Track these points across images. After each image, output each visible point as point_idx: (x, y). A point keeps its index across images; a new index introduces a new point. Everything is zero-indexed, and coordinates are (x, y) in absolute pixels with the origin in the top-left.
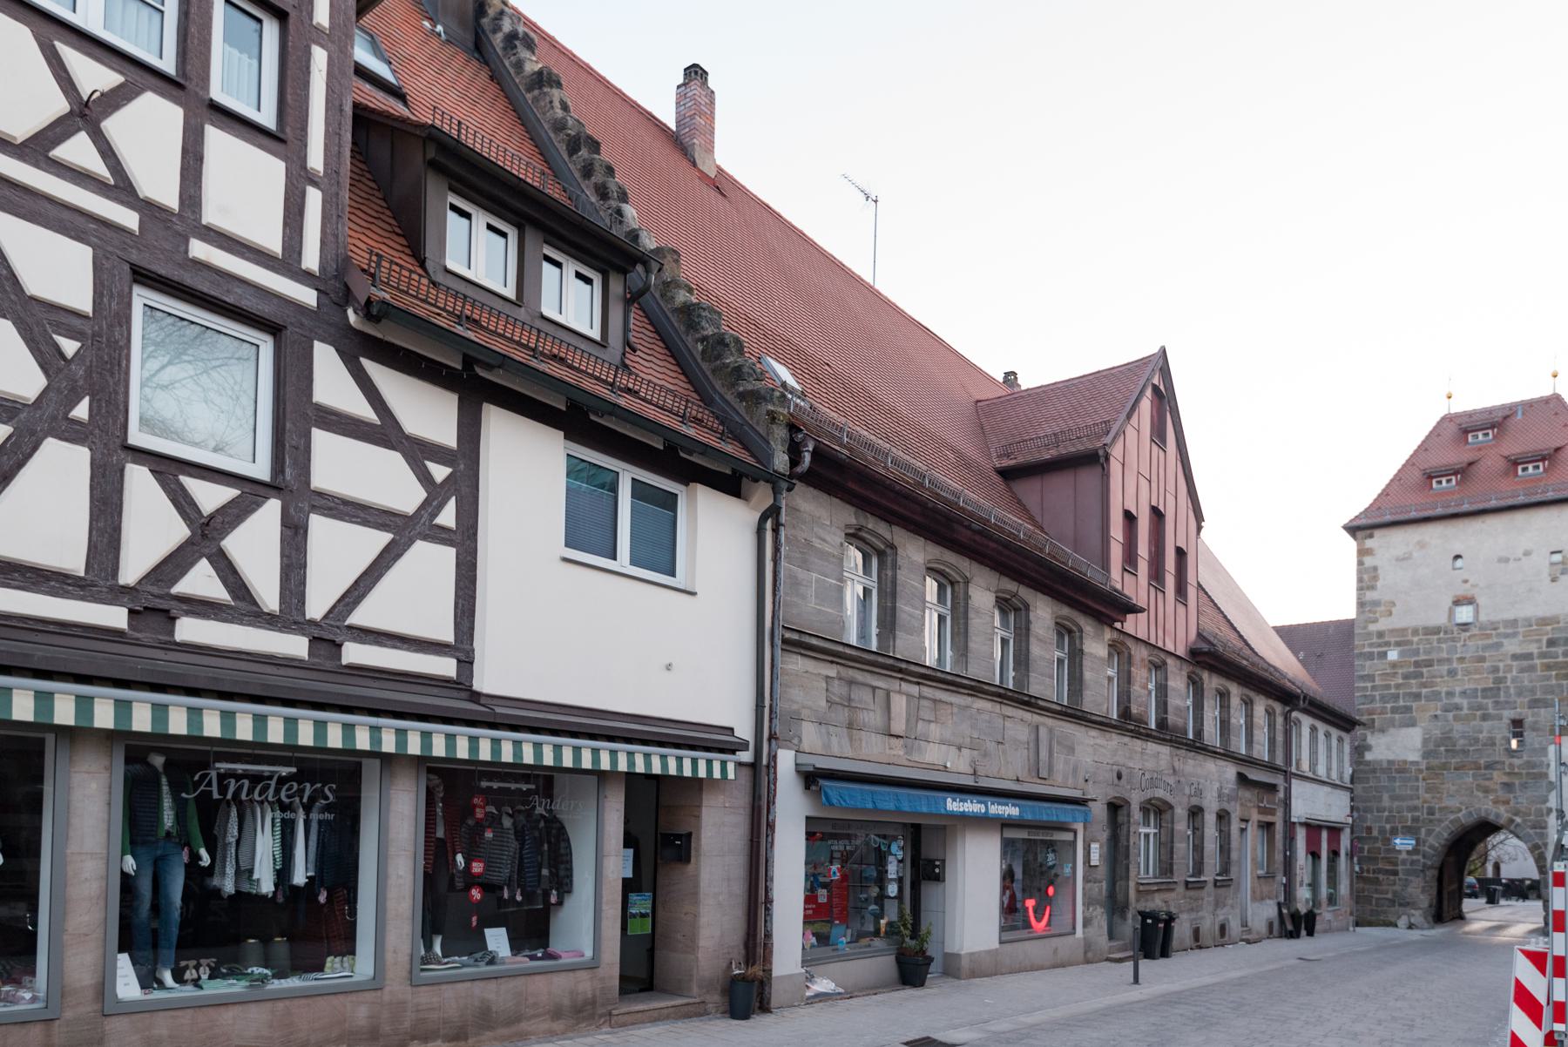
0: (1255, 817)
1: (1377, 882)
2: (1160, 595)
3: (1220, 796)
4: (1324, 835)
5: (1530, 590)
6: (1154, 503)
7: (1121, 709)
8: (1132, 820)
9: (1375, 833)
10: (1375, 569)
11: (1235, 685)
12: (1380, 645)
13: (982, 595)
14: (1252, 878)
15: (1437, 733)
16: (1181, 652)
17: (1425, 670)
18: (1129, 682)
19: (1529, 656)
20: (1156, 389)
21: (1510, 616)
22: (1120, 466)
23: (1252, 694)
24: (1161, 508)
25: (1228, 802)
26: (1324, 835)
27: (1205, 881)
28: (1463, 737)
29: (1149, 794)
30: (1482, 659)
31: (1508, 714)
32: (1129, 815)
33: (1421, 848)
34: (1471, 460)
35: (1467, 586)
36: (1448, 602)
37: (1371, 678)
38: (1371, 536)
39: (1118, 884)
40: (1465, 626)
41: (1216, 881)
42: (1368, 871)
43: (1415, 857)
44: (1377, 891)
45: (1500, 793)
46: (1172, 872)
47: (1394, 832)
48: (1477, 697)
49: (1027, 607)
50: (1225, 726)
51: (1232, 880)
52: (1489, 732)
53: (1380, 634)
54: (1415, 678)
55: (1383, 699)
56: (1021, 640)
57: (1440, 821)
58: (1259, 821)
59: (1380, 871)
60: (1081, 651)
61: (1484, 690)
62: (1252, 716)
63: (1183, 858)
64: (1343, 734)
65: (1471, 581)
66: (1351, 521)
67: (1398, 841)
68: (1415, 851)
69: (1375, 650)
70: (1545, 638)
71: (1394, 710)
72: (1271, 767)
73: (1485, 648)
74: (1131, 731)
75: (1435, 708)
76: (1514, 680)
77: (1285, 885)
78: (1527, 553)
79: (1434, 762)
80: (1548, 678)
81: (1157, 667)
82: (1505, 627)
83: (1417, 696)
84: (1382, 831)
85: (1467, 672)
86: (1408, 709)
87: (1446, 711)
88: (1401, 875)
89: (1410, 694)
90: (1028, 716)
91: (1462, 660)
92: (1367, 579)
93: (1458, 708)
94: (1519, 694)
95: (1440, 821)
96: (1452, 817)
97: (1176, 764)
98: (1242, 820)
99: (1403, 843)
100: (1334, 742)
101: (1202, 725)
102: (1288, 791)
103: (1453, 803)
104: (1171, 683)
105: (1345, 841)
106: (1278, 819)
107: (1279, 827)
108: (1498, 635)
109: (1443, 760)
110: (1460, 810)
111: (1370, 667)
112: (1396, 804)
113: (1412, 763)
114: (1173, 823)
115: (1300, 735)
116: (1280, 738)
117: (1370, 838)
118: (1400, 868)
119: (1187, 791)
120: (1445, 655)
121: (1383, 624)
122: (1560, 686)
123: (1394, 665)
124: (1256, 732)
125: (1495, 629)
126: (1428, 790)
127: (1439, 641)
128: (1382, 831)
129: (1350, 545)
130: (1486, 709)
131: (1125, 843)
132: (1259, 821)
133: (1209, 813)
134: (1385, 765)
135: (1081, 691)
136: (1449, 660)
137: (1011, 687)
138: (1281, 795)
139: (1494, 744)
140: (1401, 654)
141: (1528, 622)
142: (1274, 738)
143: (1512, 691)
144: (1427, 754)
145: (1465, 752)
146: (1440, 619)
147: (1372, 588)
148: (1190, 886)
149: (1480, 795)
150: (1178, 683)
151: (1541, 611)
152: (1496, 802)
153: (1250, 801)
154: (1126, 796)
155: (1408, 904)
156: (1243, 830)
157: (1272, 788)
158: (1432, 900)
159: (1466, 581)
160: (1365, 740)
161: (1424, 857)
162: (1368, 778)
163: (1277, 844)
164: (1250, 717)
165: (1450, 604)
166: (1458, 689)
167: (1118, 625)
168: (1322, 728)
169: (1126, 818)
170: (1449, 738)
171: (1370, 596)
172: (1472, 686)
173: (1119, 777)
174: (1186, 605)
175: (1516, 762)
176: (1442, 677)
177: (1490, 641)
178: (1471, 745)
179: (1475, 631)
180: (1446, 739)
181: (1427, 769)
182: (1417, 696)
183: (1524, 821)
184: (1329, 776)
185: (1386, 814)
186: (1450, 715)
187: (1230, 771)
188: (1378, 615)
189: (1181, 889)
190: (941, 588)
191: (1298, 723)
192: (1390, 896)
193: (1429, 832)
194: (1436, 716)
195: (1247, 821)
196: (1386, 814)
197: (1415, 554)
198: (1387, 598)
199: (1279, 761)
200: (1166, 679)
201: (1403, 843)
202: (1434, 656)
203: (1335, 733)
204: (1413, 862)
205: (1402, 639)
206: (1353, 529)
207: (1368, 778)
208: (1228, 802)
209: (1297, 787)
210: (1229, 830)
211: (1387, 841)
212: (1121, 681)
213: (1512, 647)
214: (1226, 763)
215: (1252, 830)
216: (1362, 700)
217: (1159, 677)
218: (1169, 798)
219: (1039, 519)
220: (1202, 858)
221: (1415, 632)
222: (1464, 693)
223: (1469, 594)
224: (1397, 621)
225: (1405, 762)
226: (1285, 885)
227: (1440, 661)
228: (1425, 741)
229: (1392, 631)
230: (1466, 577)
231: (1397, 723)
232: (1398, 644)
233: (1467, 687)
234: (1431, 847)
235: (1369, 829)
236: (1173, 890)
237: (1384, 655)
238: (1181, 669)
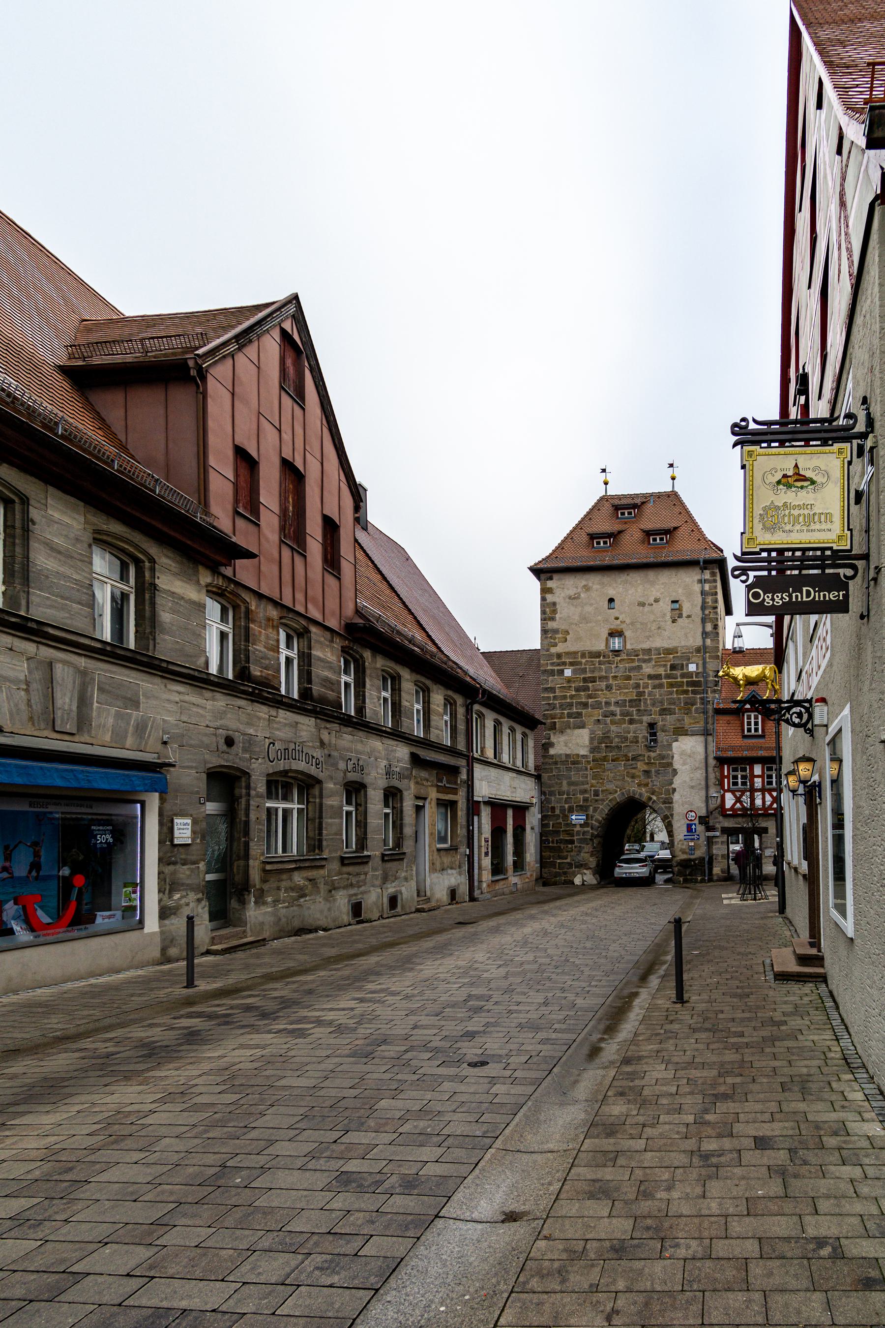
0: (433, 794)
1: (559, 850)
2: (298, 560)
3: (388, 773)
4: (510, 813)
5: (659, 628)
6: (287, 455)
7: (238, 668)
8: (253, 793)
9: (557, 812)
10: (554, 604)
11: (408, 670)
12: (559, 665)
13: (408, 684)
14: (431, 851)
15: (599, 733)
16: (333, 623)
17: (590, 685)
18: (247, 640)
19: (658, 677)
20: (285, 336)
21: (646, 646)
22: (228, 396)
23: (428, 682)
24: (299, 464)
25: (400, 779)
26: (510, 813)
27: (369, 856)
28: (617, 736)
29: (282, 765)
30: (629, 678)
31: (647, 719)
32: (248, 787)
33: (590, 821)
34: (620, 529)
35: (618, 622)
36: (605, 634)
37: (552, 690)
38: (551, 579)
39: (235, 864)
40: (617, 653)
41: (383, 855)
42: (553, 842)
43: (586, 829)
44: (560, 857)
45: (642, 778)
46: (320, 847)
47: (571, 810)
48: (626, 706)
49: (25, 501)
50: (397, 708)
51: (404, 853)
52: (634, 732)
53: (559, 656)
54: (584, 691)
55: (562, 706)
56: (14, 544)
57: (603, 800)
58: (438, 799)
59: (561, 841)
60: (154, 587)
61: (630, 701)
62: (429, 702)
63: (336, 834)
64: (527, 731)
65: (621, 619)
66: (536, 564)
67: (573, 817)
68: (586, 824)
69: (556, 668)
70: (669, 664)
71: (570, 715)
72: (452, 751)
73: (632, 669)
74: (251, 694)
75: (598, 714)
76: (650, 694)
77: (468, 856)
78: (657, 601)
79: (598, 756)
80: (671, 693)
81: (300, 635)
82: (644, 655)
83: (585, 705)
84: (562, 810)
85: (620, 688)
86: (579, 715)
87: (606, 716)
88: (576, 844)
89: (581, 703)
90: (30, 648)
91: (615, 677)
92: (548, 612)
93: (613, 714)
94: (653, 705)
95: (603, 800)
96: (611, 797)
97: (325, 736)
98: (418, 798)
99: (576, 818)
100: (519, 737)
101: (364, 701)
102: (471, 773)
103: (611, 787)
104: (316, 653)
105: (533, 819)
106: (460, 798)
107: (462, 805)
108: (639, 660)
109: (604, 754)
110: (616, 792)
111: (552, 681)
112: (572, 788)
113: (582, 756)
114: (321, 797)
115: (484, 726)
116: (461, 727)
117: (554, 816)
118: (575, 838)
119: (342, 765)
120: (604, 674)
121: (560, 648)
122: (679, 699)
123: (569, 680)
124: (433, 717)
125: (637, 655)
126: (595, 777)
127: (600, 663)
128: (562, 810)
129: (535, 584)
130: (632, 715)
131: (243, 819)
132: (438, 799)
133: (375, 789)
134: (564, 758)
135: (153, 633)
136: (606, 678)
137: (109, 640)
138: (464, 776)
139: (637, 742)
140: (573, 672)
141: (658, 651)
142: (456, 726)
143: (648, 702)
144: (593, 750)
145: (619, 748)
146: (601, 646)
147: (553, 619)
148: (346, 862)
149: (630, 780)
150: (329, 655)
151: (666, 644)
152: (639, 785)
153: (427, 780)
154: (242, 765)
155: (582, 865)
156: (419, 809)
157: (454, 771)
158: (598, 861)
159: (617, 618)
160: (549, 739)
161: (592, 828)
162: (552, 769)
163: (459, 821)
164: (427, 704)
165: (606, 635)
166: (613, 700)
167: (228, 571)
168: (506, 725)
169: (244, 791)
170: (608, 737)
171: (551, 625)
172: (622, 698)
173: (230, 742)
174: (339, 579)
175: (652, 754)
176: (602, 690)
177: (634, 665)
178: (623, 742)
179: (624, 656)
180: (606, 738)
181: (593, 761)
182: (585, 705)
183: (658, 799)
184: (514, 764)
185: (565, 796)
186: (608, 720)
187: (402, 752)
188: (557, 640)
189: (335, 865)
190: (224, 611)
191: (481, 716)
192: (568, 860)
193: (595, 810)
194: (599, 720)
195: (425, 799)
196: (565, 796)
197: (582, 595)
198: (563, 627)
199: (461, 746)
200: (310, 648)
201: (576, 818)
202: (596, 674)
203: (519, 729)
204: (584, 833)
205: (574, 658)
206: (538, 571)
207: (552, 769)
208: (400, 779)
209: (478, 770)
210: (402, 806)
211: (566, 817)
212: (237, 638)
213: (648, 669)
214: (396, 743)
215: (430, 811)
216: (547, 707)
217: (301, 644)
218: (313, 771)
219: (122, 437)
220: (365, 833)
221: (583, 655)
222: (617, 703)
223: (619, 628)
224: (570, 646)
225: (578, 755)
226: (468, 856)
227: (601, 678)
228: (592, 739)
229: (567, 653)
230: (617, 615)
231: (572, 725)
232: (571, 664)
233: (619, 698)
234: (597, 820)
235: (553, 809)
236: (322, 867)
237: (561, 672)
238: (332, 641)
